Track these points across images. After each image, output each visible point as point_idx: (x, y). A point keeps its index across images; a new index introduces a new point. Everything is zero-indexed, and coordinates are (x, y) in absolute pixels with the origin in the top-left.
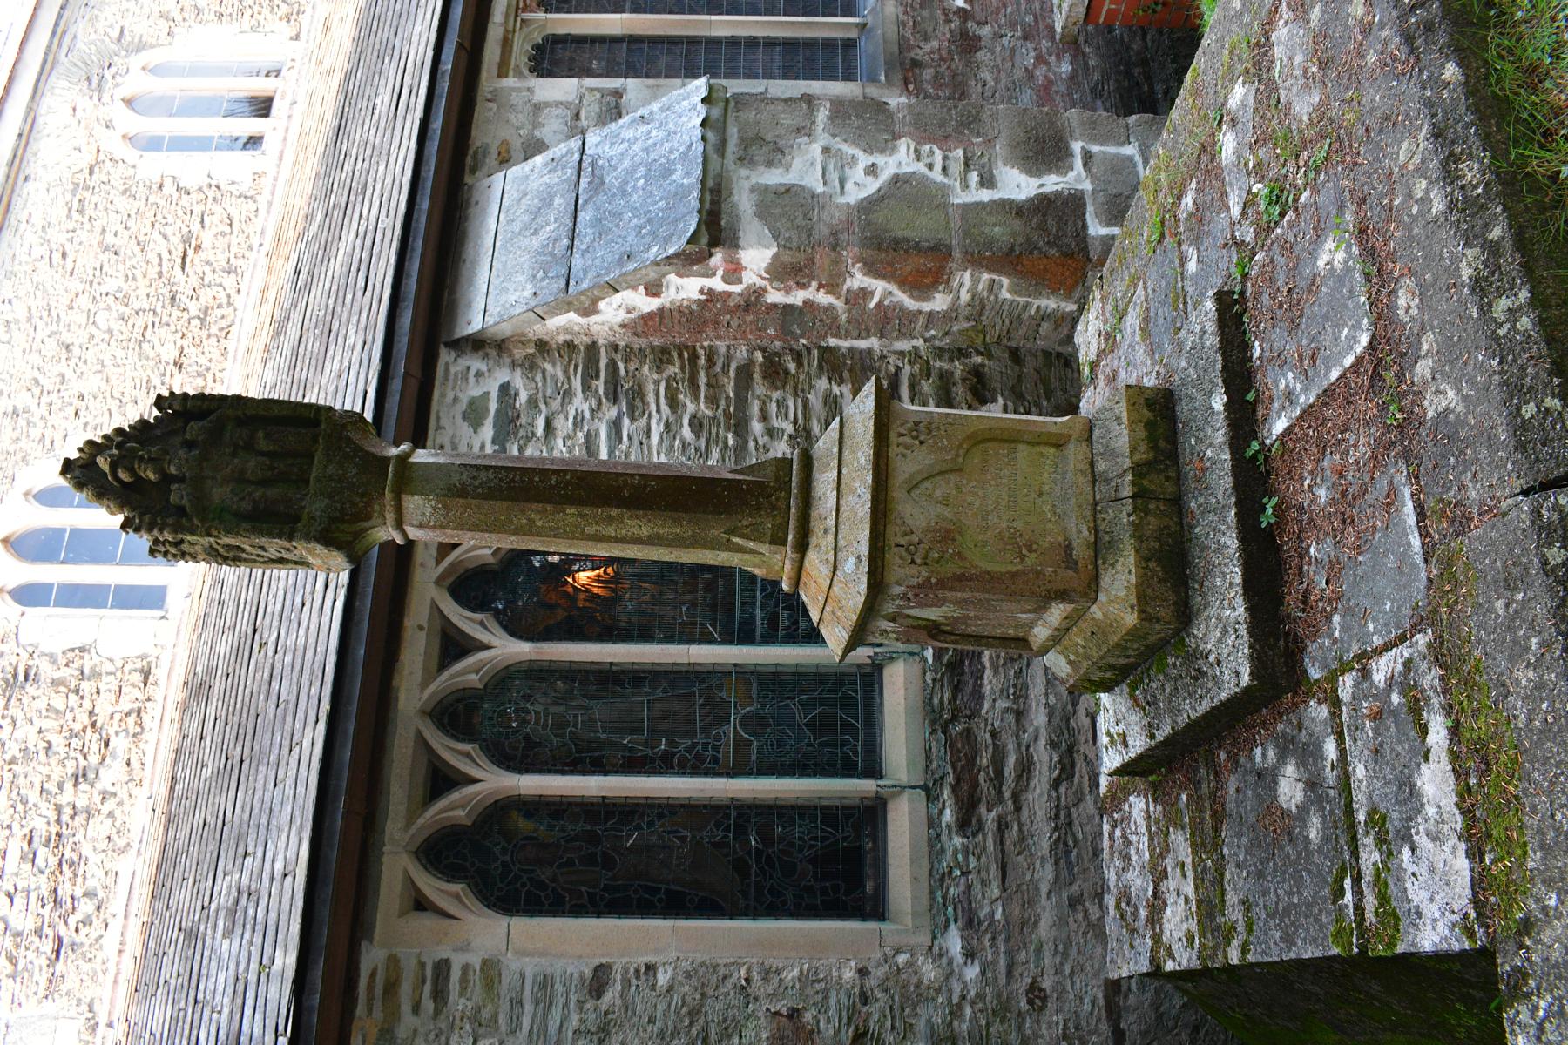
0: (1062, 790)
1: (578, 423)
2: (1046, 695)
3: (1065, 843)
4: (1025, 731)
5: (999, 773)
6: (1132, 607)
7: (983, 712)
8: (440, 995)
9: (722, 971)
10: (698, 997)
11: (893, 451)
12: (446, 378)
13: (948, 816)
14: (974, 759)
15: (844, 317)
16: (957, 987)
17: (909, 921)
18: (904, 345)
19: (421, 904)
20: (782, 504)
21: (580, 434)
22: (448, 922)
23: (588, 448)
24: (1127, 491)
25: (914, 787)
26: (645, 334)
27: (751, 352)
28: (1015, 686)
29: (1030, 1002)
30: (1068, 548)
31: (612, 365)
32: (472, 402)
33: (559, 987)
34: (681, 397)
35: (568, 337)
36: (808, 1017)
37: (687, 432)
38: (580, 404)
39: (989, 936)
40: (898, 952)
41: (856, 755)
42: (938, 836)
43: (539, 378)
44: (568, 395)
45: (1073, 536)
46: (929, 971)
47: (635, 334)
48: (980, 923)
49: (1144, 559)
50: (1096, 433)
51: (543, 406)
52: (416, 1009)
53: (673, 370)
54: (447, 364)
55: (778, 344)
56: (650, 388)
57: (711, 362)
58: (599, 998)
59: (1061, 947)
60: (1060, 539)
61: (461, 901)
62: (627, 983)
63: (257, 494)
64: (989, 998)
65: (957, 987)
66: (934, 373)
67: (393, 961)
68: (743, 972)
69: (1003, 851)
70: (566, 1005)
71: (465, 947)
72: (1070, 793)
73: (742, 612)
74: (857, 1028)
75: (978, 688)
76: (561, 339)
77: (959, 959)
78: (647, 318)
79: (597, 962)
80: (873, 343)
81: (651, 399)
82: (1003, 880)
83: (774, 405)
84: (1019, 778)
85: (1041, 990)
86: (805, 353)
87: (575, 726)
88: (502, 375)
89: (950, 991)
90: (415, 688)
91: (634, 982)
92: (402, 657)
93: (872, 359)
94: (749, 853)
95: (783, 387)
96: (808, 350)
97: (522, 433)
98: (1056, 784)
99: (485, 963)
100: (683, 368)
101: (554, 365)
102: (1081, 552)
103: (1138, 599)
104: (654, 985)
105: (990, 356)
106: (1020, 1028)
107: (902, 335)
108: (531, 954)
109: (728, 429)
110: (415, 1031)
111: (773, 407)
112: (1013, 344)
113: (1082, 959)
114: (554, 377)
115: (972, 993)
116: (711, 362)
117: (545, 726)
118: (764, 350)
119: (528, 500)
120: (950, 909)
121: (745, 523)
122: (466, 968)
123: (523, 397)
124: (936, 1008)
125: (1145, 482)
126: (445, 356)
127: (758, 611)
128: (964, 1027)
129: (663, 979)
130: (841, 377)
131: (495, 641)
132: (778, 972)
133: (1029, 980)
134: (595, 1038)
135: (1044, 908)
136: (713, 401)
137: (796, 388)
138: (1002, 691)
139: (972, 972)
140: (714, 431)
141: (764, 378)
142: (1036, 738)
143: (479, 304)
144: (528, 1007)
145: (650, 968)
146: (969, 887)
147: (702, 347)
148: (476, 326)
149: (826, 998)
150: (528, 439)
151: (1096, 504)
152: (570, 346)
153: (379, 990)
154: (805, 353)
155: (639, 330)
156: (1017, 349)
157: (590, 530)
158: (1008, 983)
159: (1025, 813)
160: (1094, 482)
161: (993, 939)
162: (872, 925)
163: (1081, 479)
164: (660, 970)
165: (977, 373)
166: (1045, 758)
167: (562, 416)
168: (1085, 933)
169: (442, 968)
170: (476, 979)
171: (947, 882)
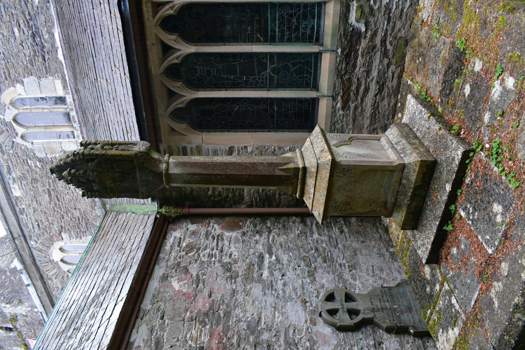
0: (378, 97)
2: (379, 66)
3: (375, 113)
4: (369, 78)
5: (358, 92)
7: (356, 71)
9: (266, 148)
11: (335, 178)
13: (339, 105)
14: (350, 87)
22: (183, 137)
25: (329, 96)
28: (368, 62)
30: (386, 203)
41: (310, 81)
42: (335, 111)
45: (389, 200)
49: (407, 214)
50: (406, 170)
68: (273, 148)
69: (355, 116)
72: (380, 98)
73: (271, 32)
75: (355, 62)
79: (230, 146)
82: (354, 124)
84: (364, 93)
87: (214, 73)
90: (157, 68)
91: (241, 151)
92: (149, 56)
94: (274, 111)
98: (376, 96)
99: (197, 147)
102: (389, 205)
103: (403, 224)
104: (247, 152)
117: (203, 73)
122: (191, 148)
125: (416, 192)
127: (277, 29)
129: (249, 150)
131: (181, 48)
132: (283, 148)
138: (363, 64)
142: (372, 80)
145: (246, 147)
146: (343, 126)
159: (364, 103)
160: (400, 184)
164: (248, 148)
166: (374, 88)
171: (336, 124)
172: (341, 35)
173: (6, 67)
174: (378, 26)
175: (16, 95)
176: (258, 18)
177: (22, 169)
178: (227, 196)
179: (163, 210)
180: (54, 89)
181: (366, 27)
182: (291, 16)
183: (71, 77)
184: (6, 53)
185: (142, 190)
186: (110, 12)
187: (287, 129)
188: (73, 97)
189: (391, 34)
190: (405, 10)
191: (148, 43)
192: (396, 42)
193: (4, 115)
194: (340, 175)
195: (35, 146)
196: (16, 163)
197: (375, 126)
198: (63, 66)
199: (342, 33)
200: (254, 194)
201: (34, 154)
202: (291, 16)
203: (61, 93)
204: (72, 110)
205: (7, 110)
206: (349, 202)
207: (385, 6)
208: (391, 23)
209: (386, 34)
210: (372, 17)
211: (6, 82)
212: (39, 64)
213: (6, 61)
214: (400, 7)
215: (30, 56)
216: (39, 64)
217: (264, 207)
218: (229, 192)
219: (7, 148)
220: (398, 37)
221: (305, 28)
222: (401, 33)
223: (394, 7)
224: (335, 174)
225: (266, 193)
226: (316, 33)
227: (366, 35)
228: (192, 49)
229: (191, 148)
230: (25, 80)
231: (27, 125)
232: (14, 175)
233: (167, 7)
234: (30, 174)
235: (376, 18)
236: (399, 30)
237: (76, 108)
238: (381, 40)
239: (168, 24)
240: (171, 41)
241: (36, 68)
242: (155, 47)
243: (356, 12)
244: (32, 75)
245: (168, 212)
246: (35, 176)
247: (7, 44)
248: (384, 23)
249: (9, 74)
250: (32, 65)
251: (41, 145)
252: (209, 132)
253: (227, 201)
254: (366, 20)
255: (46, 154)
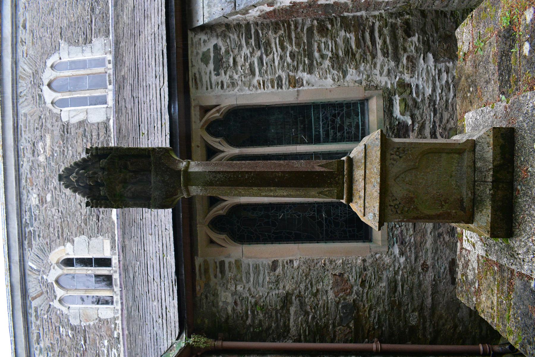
1: (246, 59)
6: (488, 232)
8: (222, 272)
10: (308, 270)
11: (388, 162)
12: (192, 44)
15: (351, 6)
16: (397, 265)
17: (380, 243)
18: (377, 13)
19: (212, 242)
20: (341, 182)
21: (247, 64)
23: (251, 70)
24: (490, 179)
26: (268, 18)
27: (312, 21)
29: (423, 269)
30: (462, 201)
31: (257, 32)
32: (204, 54)
33: (261, 268)
34: (285, 44)
35: (238, 22)
36: (346, 275)
37: (289, 59)
38: (246, 51)
39: (408, 247)
40: (376, 254)
43: (228, 41)
44: (240, 47)
45: (465, 196)
46: (387, 260)
47: (264, 18)
48: (406, 243)
50: (478, 148)
51: (231, 53)
52: (215, 276)
53: (282, 32)
54: (192, 38)
55: (323, 16)
56: (273, 41)
57: (296, 27)
58: (275, 271)
59: (434, 251)
60: (459, 197)
61: (221, 144)
62: (284, 266)
63: (133, 190)
64: (408, 268)
65: (397, 265)
66: (389, 24)
67: (205, 262)
68: (323, 261)
70: (264, 274)
71: (229, 256)
73: (315, 131)
74: (362, 279)
76: (235, 23)
77: (398, 256)
78: (268, 13)
79: (273, 259)
80: (363, 13)
81: (273, 45)
82: (414, 229)
83: (323, 44)
85: (426, 265)
86: (334, 20)
88: (214, 41)
89: (395, 266)
91: (286, 265)
93: (362, 20)
94: (323, 219)
95: (326, 36)
96: (336, 18)
97: (225, 65)
99: (236, 261)
100: (285, 31)
101: (233, 34)
103: (491, 228)
104: (293, 267)
105: (412, 15)
106: (419, 277)
107: (375, 9)
108: (251, 258)
109: (305, 57)
110: (216, 283)
111: (323, 46)
112: (422, 9)
113: (442, 254)
114: (234, 39)
115: (402, 267)
116: (296, 27)
118: (317, 20)
119: (237, 186)
120: (395, 239)
121: (325, 189)
122: (230, 263)
123: (223, 50)
124: (390, 271)
125: (498, 175)
126: (190, 35)
127: (321, 130)
128: (399, 277)
129: (296, 264)
130: (350, 30)
132: (335, 261)
133: (423, 262)
134: (275, 284)
135: (429, 237)
136: (298, 45)
137: (331, 36)
139: (402, 260)
140: (300, 58)
141: (318, 32)
143: (200, 12)
144: (252, 275)
145: (291, 261)
146: (402, 231)
147: (292, 21)
148: (201, 23)
149: (352, 269)
150: (227, 68)
151: (475, 181)
152: (239, 25)
153: (203, 271)
154: (334, 20)
155: (266, 17)
156: (424, 11)
157: (264, 194)
158: (415, 263)
161: (410, 248)
162: (367, 244)
163: (469, 170)
164: (295, 262)
165: (407, 23)
167: (239, 56)
168: (443, 246)
169: (222, 263)
170: (234, 266)
171: (394, 229)
172: (387, 129)
173: (61, 226)
174: (425, 118)
175: (64, 254)
176: (301, 118)
177: (52, 338)
178: (270, 327)
179: (191, 341)
180: (102, 249)
181: (412, 120)
182: (334, 116)
183: (120, 237)
184: (64, 212)
185: (155, 194)
186: (161, 113)
187: (339, 240)
188: (119, 258)
189: (440, 126)
190: (450, 101)
191: (193, 145)
192: (447, 133)
193: (48, 275)
194: (395, 157)
195: (71, 311)
196: (47, 330)
197: (440, 230)
198: (114, 226)
199: (388, 127)
200: (302, 325)
201: (68, 320)
202: (334, 116)
203: (107, 254)
204: (115, 272)
205: (52, 270)
206: (412, 198)
207: (428, 98)
208: (438, 115)
209: (434, 126)
210: (416, 109)
211: (58, 241)
212: (93, 223)
213: (63, 220)
214: (444, 98)
215: (85, 215)
216: (93, 223)
217: (314, 342)
218: (272, 321)
219: (42, 312)
220: (448, 128)
221: (350, 126)
222: (450, 124)
223: (438, 98)
224: (388, 156)
225: (317, 323)
226: (362, 130)
227: (413, 128)
228: (236, 151)
229: (230, 263)
230: (76, 239)
231: (68, 287)
232: (42, 345)
233: (214, 110)
234: (59, 345)
235: (421, 111)
236: (448, 121)
237: (120, 270)
238: (431, 132)
239: (213, 128)
240: (216, 143)
241: (88, 227)
242: (199, 149)
243: (400, 106)
244: (83, 234)
245: (197, 342)
246: (64, 347)
247: (67, 203)
248: (430, 115)
249: (62, 233)
250: (86, 224)
251: (77, 311)
252: (250, 244)
253: (270, 334)
254: (411, 112)
255: (81, 321)
